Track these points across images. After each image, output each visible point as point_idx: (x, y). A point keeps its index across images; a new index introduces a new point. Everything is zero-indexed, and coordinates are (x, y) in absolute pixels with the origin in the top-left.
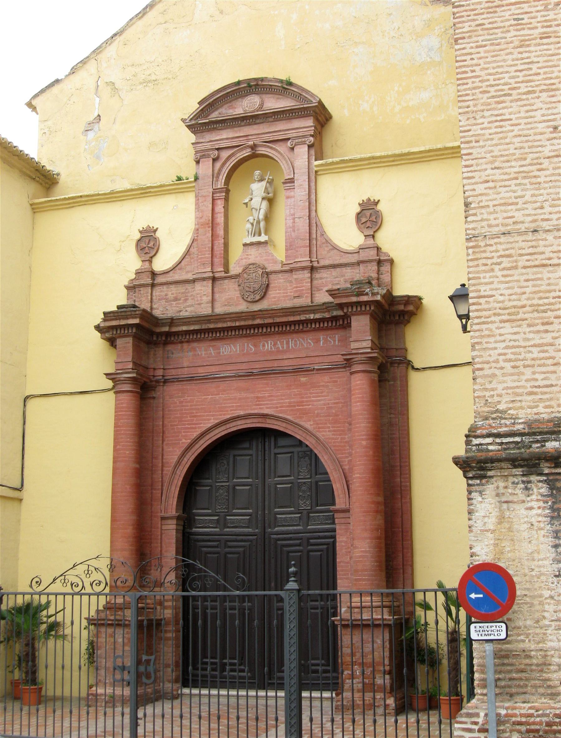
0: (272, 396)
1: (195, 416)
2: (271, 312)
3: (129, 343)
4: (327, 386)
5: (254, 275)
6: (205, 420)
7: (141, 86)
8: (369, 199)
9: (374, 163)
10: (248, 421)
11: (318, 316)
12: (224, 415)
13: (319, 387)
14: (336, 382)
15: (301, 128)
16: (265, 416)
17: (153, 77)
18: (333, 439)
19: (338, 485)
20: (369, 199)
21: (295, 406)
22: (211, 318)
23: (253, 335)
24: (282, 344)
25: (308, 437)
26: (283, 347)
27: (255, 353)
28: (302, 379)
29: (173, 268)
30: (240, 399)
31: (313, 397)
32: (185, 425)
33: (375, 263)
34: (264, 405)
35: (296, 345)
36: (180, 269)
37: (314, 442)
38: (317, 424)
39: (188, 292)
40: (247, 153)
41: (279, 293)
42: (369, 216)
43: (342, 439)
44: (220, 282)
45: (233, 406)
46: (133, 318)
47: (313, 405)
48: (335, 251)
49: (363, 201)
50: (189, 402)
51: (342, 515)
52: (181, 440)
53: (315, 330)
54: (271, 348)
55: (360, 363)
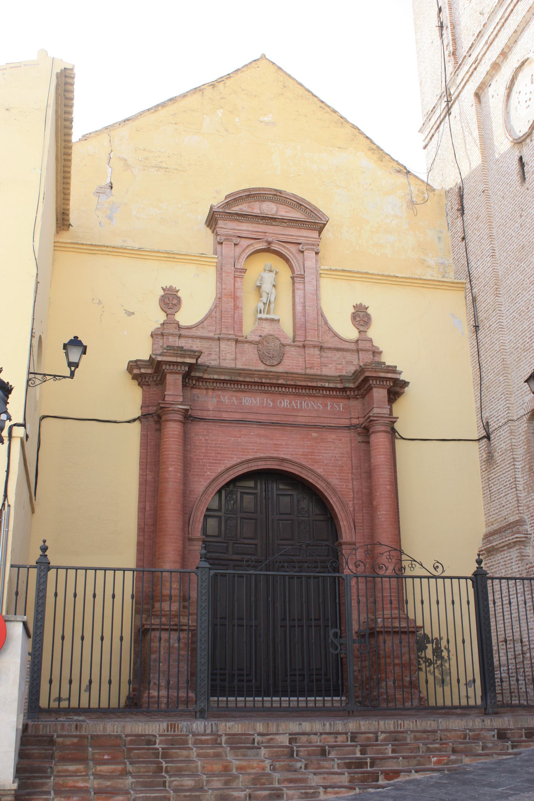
0: (288, 445)
1: (219, 453)
2: (295, 376)
3: (178, 379)
4: (334, 443)
5: (273, 344)
6: (229, 457)
7: (153, 169)
8: (361, 304)
9: (365, 278)
10: (269, 463)
11: (331, 385)
12: (246, 455)
13: (328, 442)
14: (341, 440)
15: (310, 238)
16: (283, 460)
17: (164, 165)
18: (339, 485)
19: (345, 523)
20: (361, 304)
21: (307, 455)
22: (242, 372)
23: (272, 393)
24: (296, 403)
25: (319, 482)
26: (297, 407)
27: (273, 407)
28: (313, 434)
29: (196, 326)
30: (260, 443)
31: (323, 450)
32: (210, 460)
33: (371, 353)
34: (282, 451)
35: (308, 406)
36: (203, 328)
37: (324, 485)
38: (326, 472)
39: (212, 348)
40: (263, 246)
41: (292, 363)
42: (361, 317)
43: (346, 485)
44: (240, 345)
45: (254, 449)
46: (190, 357)
47: (322, 456)
48: (336, 338)
49: (357, 304)
50: (214, 440)
51: (348, 547)
52: (206, 472)
53: (324, 396)
54: (287, 406)
55: (383, 425)
